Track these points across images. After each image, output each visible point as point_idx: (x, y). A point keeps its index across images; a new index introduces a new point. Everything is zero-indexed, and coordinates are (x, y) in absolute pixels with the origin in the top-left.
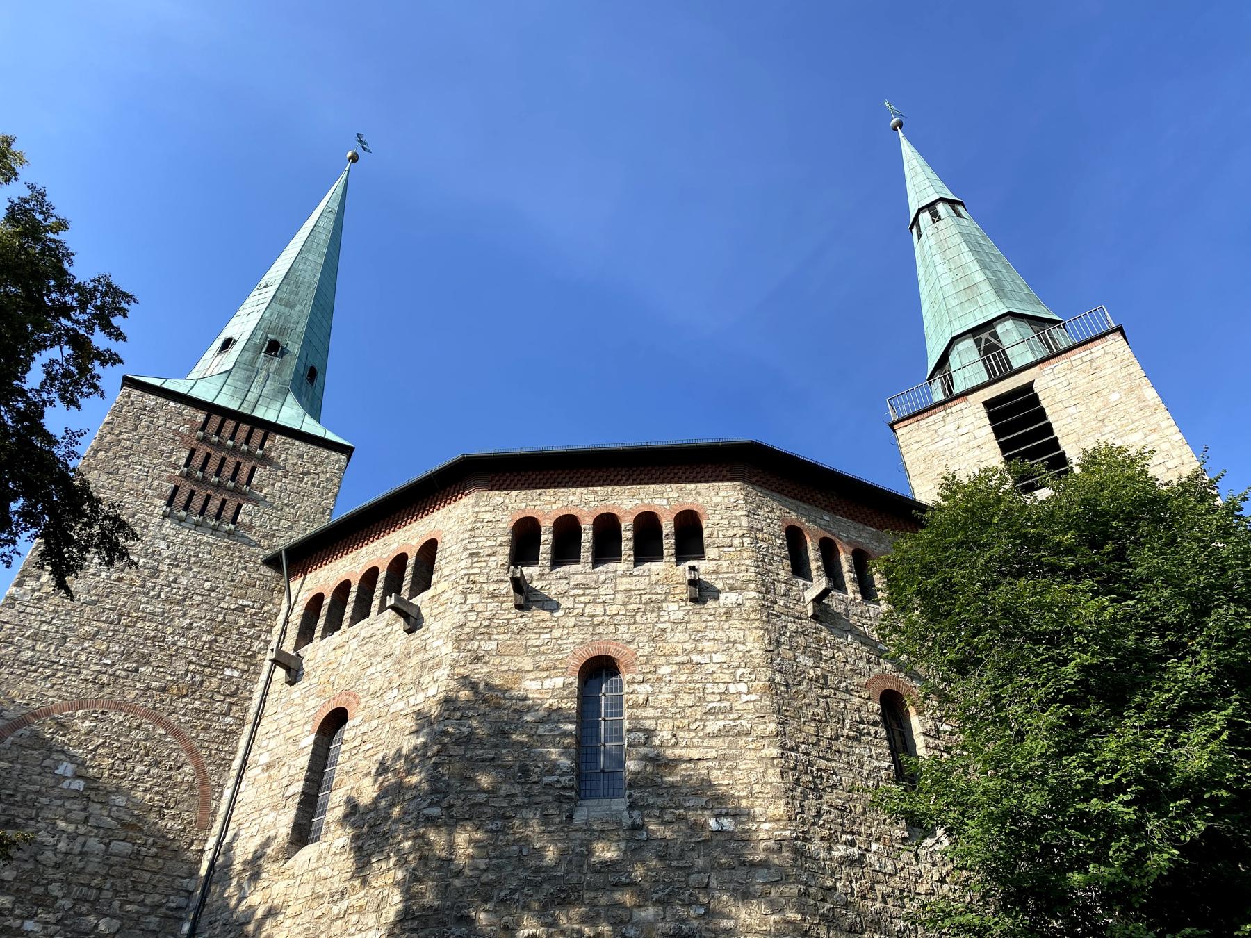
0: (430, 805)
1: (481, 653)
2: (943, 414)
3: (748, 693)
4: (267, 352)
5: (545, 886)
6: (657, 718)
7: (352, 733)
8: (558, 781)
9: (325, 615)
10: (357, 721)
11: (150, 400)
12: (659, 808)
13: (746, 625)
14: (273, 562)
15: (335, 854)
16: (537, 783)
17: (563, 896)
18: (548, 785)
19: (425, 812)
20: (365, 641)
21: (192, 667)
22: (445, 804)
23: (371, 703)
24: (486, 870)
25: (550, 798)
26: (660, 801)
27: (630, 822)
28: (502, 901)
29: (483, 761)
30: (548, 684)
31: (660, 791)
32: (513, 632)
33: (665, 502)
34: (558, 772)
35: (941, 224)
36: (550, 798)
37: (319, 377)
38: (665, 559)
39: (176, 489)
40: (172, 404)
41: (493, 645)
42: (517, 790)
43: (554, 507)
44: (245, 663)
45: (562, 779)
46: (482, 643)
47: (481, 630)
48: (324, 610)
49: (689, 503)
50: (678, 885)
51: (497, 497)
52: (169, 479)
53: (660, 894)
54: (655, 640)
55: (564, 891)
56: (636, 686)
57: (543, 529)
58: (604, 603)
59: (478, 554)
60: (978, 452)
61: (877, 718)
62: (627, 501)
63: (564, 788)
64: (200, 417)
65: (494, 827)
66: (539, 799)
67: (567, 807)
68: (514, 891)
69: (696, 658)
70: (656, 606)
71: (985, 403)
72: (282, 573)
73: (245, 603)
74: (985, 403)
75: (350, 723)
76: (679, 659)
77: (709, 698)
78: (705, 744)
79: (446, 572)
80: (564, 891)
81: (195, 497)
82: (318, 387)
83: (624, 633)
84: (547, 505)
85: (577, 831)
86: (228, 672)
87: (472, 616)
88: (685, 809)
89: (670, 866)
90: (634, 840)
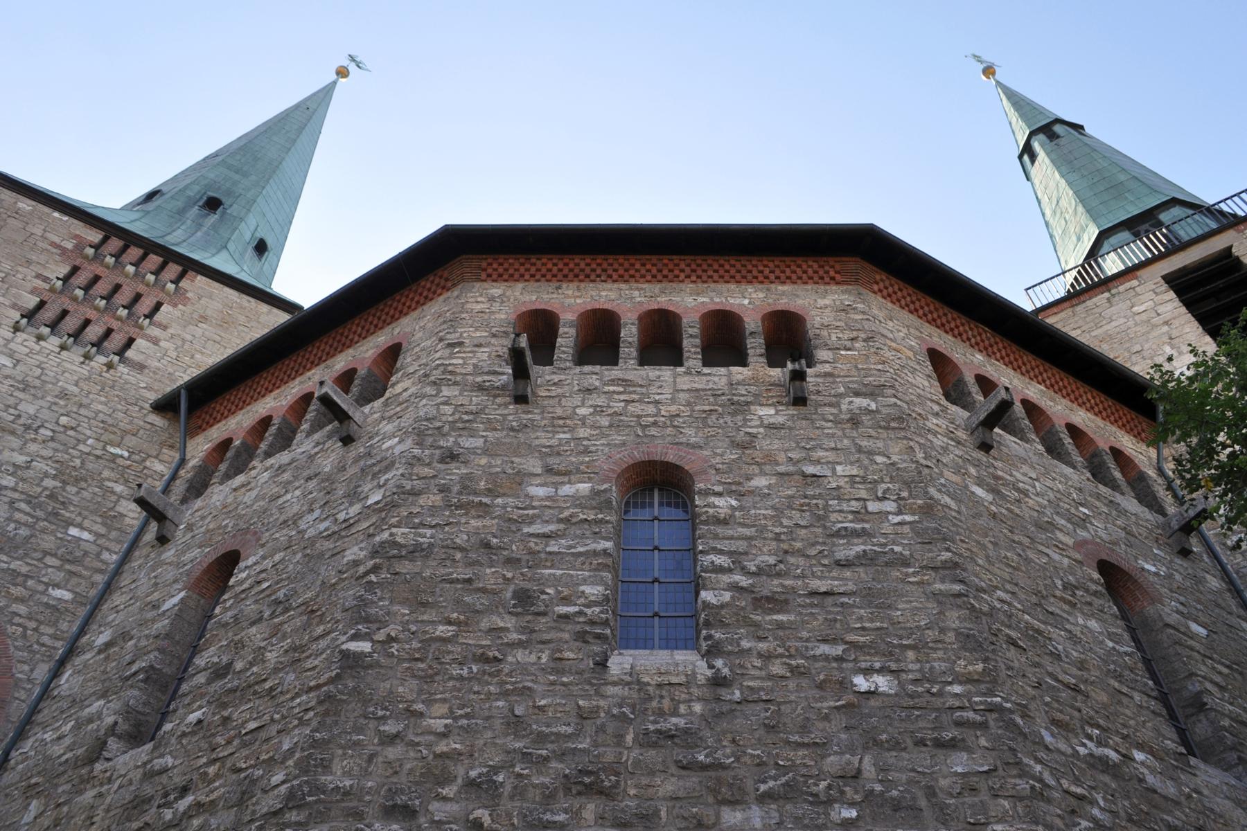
0: (355, 637)
1: (456, 450)
2: (1107, 295)
3: (899, 513)
4: (202, 207)
5: (554, 764)
6: (748, 538)
7: (244, 575)
8: (580, 613)
9: (231, 458)
10: (250, 561)
11: (25, 205)
12: (760, 655)
13: (884, 434)
14: (166, 406)
15: (184, 735)
16: (544, 614)
17: (587, 780)
18: (566, 617)
19: (344, 647)
20: (281, 469)
21: (18, 516)
22: (381, 636)
23: (277, 535)
24: (444, 735)
25: (566, 636)
26: (762, 646)
27: (709, 673)
28: (471, 784)
29: (452, 582)
30: (567, 490)
31: (760, 633)
32: (512, 429)
33: (746, 302)
34: (582, 600)
35: (1062, 141)
36: (566, 636)
37: (269, 256)
38: (751, 359)
39: (42, 304)
40: (56, 214)
41: (479, 442)
42: (509, 622)
43: (578, 301)
44: (104, 524)
45: (589, 611)
46: (460, 440)
47: (460, 425)
48: (229, 454)
49: (784, 304)
50: (804, 771)
51: (496, 290)
52: (34, 291)
53: (771, 784)
54: (743, 446)
55: (589, 773)
56: (713, 499)
57: (562, 322)
58: (657, 402)
59: (461, 344)
60: (1166, 328)
61: (1100, 588)
62: (691, 300)
63: (592, 623)
64: (95, 236)
65: (465, 672)
66: (547, 637)
67: (597, 649)
68: (495, 770)
69: (810, 469)
70: (740, 408)
71: (1164, 277)
72: (178, 421)
73: (118, 451)
74: (1164, 277)
75: (242, 565)
76: (781, 469)
77: (834, 517)
78: (834, 574)
79: (411, 370)
80: (589, 773)
81: (67, 318)
82: (266, 266)
83: (691, 434)
84: (571, 300)
85: (614, 684)
86: (73, 531)
87: (448, 409)
88: (807, 658)
89: (788, 743)
90: (718, 699)
